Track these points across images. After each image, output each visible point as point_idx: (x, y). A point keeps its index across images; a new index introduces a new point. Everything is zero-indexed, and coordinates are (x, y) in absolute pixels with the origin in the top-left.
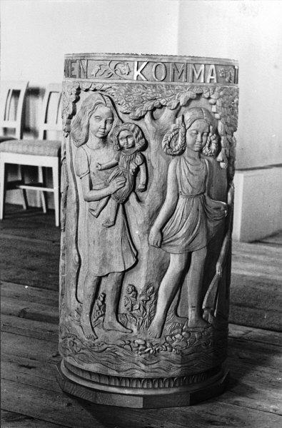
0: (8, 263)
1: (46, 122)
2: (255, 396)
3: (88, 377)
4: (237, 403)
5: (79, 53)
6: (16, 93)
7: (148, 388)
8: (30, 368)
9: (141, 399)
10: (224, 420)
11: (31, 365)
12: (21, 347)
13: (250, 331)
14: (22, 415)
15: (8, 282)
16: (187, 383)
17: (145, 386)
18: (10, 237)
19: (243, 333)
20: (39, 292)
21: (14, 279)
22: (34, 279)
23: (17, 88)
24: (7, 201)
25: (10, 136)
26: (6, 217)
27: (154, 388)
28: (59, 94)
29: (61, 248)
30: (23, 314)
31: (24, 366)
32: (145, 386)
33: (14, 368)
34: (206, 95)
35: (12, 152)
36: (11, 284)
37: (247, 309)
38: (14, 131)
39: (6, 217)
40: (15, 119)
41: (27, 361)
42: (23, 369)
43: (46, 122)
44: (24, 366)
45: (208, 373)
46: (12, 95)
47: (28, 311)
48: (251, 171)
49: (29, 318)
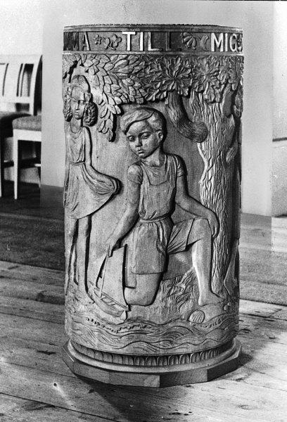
0: (23, 245)
1: (3, 94)
2: (268, 372)
3: (84, 351)
4: (267, 386)
5: (155, 23)
6: (29, 68)
7: (140, 366)
8: (50, 354)
9: (158, 378)
10: (255, 403)
11: (49, 351)
12: (38, 332)
13: (280, 310)
14: (42, 403)
15: (24, 264)
16: (194, 361)
17: (161, 364)
18: (26, 217)
19: (272, 311)
20: (58, 275)
21: (32, 261)
22: (51, 260)
23: (29, 62)
24: (22, 180)
25: (24, 112)
26: (21, 196)
27: (134, 366)
28: (5, 66)
29: (263, 248)
30: (41, 298)
31: (43, 352)
32: (161, 364)
33: (33, 352)
34: (80, 63)
35: (26, 129)
36: (27, 267)
37: (275, 286)
38: (27, 106)
39: (21, 196)
40: (29, 95)
41: (45, 347)
42: (42, 355)
43: (3, 94)
44: (43, 352)
45: (221, 349)
46: (25, 69)
47: (45, 294)
48: (278, 142)
49: (47, 302)
